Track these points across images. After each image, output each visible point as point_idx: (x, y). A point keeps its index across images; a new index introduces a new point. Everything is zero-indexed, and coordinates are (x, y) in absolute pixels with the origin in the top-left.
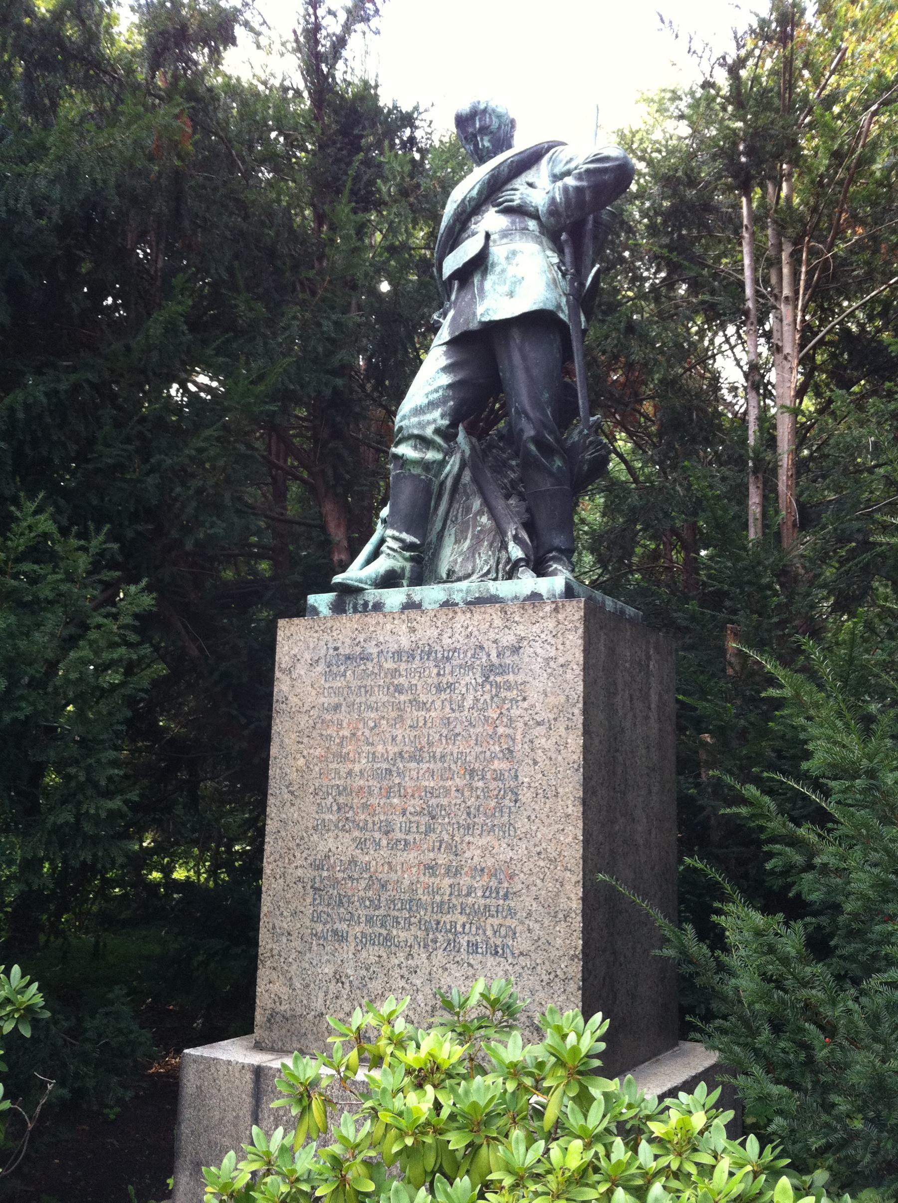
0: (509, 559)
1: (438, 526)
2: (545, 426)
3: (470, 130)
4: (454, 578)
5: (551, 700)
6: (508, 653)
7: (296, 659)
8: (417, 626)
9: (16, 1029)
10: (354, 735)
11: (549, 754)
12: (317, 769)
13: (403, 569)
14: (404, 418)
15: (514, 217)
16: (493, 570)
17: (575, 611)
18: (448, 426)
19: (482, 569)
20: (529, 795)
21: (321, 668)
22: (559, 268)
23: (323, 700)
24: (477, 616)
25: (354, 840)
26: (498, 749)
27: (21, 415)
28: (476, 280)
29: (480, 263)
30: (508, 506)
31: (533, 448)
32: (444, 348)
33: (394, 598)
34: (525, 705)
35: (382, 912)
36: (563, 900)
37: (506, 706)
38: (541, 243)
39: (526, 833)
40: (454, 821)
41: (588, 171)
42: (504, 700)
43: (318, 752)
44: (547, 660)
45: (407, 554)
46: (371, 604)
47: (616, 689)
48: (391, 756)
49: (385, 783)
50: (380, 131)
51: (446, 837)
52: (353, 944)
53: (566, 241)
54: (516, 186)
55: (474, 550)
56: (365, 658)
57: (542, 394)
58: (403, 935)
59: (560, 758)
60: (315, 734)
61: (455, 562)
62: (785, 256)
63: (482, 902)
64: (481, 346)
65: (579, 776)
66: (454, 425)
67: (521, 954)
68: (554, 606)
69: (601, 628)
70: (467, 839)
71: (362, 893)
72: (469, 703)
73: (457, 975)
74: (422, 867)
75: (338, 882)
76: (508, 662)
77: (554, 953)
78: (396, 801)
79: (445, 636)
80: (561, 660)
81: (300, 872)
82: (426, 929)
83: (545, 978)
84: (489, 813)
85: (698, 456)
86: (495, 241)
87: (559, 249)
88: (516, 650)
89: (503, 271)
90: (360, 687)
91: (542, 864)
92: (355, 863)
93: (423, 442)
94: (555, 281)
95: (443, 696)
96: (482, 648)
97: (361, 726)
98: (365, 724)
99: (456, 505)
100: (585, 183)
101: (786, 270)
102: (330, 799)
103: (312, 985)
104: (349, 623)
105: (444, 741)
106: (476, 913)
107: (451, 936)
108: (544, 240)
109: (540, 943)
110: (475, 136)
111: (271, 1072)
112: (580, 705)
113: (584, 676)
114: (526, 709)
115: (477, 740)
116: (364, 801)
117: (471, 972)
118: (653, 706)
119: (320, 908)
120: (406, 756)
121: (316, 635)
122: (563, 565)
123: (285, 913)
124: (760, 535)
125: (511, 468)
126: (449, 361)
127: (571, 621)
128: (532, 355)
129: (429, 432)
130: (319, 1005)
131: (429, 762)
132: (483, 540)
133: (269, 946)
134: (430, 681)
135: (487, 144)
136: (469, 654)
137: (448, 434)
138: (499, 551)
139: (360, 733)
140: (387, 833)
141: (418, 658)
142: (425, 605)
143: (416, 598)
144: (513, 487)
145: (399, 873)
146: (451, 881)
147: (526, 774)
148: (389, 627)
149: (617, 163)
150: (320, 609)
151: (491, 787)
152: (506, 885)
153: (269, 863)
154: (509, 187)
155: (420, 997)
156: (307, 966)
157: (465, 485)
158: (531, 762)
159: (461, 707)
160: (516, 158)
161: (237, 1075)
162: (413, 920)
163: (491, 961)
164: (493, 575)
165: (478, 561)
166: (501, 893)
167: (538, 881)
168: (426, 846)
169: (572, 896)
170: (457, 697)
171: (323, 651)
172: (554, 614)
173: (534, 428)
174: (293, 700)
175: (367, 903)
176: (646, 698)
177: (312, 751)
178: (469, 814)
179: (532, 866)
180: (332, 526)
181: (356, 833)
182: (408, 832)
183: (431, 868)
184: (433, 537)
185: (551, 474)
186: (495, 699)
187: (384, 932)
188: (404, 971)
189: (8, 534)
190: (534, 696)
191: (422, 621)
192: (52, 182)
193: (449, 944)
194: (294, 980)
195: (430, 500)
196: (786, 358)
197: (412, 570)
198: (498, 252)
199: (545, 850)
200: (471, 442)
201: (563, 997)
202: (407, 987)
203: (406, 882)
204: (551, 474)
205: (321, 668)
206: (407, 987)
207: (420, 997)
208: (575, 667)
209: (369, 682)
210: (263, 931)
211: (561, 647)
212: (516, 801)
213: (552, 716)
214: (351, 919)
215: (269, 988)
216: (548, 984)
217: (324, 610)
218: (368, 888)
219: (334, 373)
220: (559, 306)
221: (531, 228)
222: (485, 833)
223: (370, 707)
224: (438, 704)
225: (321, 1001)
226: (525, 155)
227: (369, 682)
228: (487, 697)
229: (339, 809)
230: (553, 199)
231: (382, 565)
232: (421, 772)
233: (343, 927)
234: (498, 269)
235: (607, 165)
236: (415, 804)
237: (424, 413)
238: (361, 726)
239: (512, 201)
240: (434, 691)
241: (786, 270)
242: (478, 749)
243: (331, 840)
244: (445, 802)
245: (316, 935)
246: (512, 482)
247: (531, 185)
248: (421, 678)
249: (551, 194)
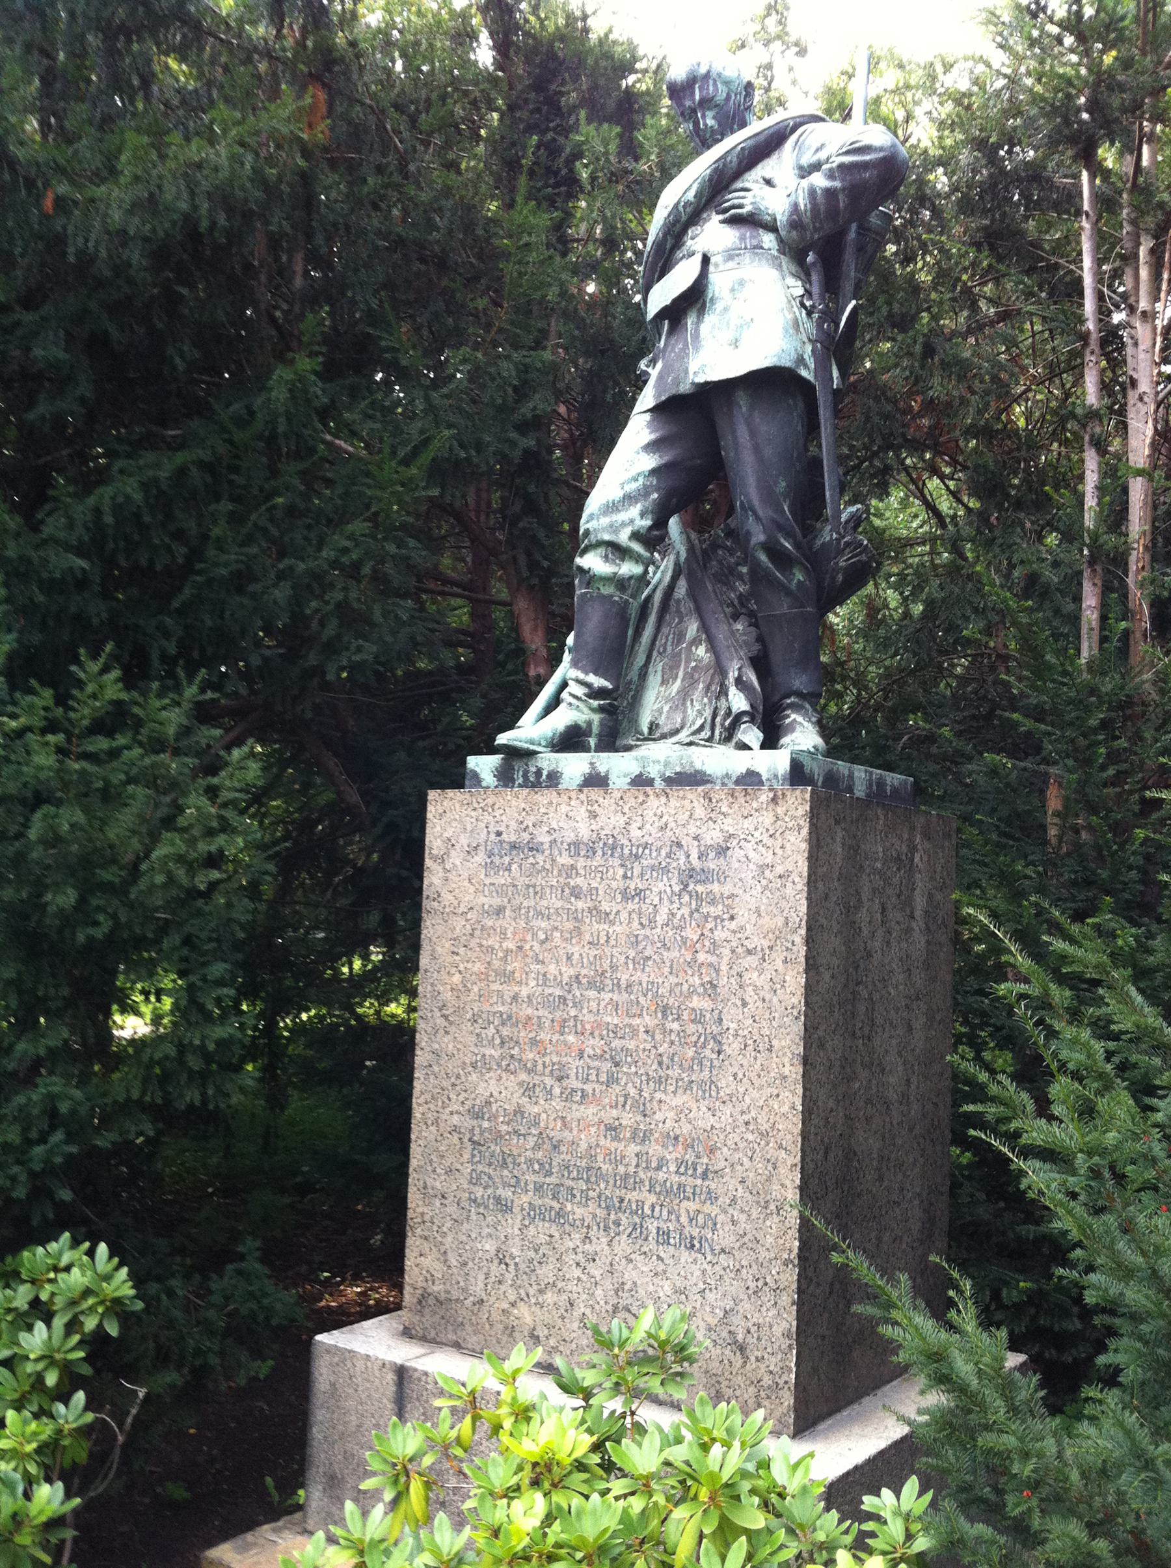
0: (729, 712)
1: (640, 659)
2: (780, 528)
3: (688, 103)
4: (657, 735)
5: (766, 921)
6: (712, 855)
8: (599, 811)
9: (100, 1326)
10: (520, 948)
11: (762, 994)
12: (476, 989)
13: (589, 723)
14: (591, 517)
15: (743, 230)
16: (708, 726)
17: (798, 803)
18: (650, 528)
21: (480, 858)
22: (803, 305)
23: (483, 900)
24: (673, 802)
25: (521, 1084)
26: (698, 982)
27: (109, 519)
28: (690, 321)
29: (694, 298)
30: (733, 633)
31: (763, 557)
32: (647, 417)
33: (574, 766)
34: (733, 925)
35: (553, 1179)
37: (709, 926)
38: (779, 267)
39: (731, 1096)
40: (642, 1071)
41: (842, 166)
42: (706, 917)
43: (478, 967)
44: (762, 868)
45: (595, 703)
46: (545, 773)
47: (859, 900)
48: (565, 979)
49: (558, 1014)
50: (584, 87)
51: (633, 1092)
52: (520, 1217)
53: (813, 264)
54: (747, 185)
55: (685, 694)
56: (534, 848)
57: (776, 483)
58: (579, 1212)
59: (775, 1000)
60: (473, 943)
61: (660, 711)
62: (1143, 252)
63: (676, 1179)
64: (697, 413)
65: (799, 1027)
66: (660, 523)
67: (723, 1251)
68: (771, 795)
69: (837, 822)
70: (658, 1095)
71: (528, 1153)
72: (662, 918)
73: (645, 1269)
74: (602, 1127)
75: (501, 1137)
76: (712, 866)
77: (764, 1255)
78: (571, 1038)
79: (634, 826)
80: (780, 870)
81: (455, 1119)
82: (607, 1207)
83: (752, 1285)
84: (686, 1065)
85: (1023, 528)
86: (716, 265)
87: (804, 272)
88: (722, 851)
89: (726, 309)
90: (528, 886)
91: (751, 1137)
92: (522, 1113)
93: (618, 551)
94: (796, 324)
95: (631, 906)
96: (679, 845)
97: (529, 937)
98: (535, 935)
99: (665, 630)
100: (837, 184)
101: (1144, 273)
102: (492, 1030)
103: (470, 1264)
104: (515, 801)
105: (631, 966)
106: (667, 1192)
107: (637, 1220)
108: (784, 260)
109: (746, 1239)
110: (694, 111)
111: (416, 1375)
112: (803, 932)
113: (809, 893)
114: (734, 932)
115: (671, 967)
116: (532, 1035)
117: (661, 1267)
118: (918, 913)
119: (480, 1168)
120: (584, 981)
121: (474, 814)
122: (805, 715)
123: (439, 1170)
124: (1096, 652)
125: (740, 577)
126: (653, 437)
127: (793, 818)
128: (764, 428)
129: (623, 537)
130: (478, 1288)
131: (612, 991)
132: (697, 681)
133: (420, 1210)
134: (614, 884)
135: (710, 122)
136: (663, 853)
137: (653, 538)
138: (718, 698)
139: (527, 947)
140: (560, 1079)
141: (600, 852)
142: (613, 778)
143: (602, 769)
144: (742, 605)
145: (575, 1132)
146: (638, 1148)
147: (732, 1017)
148: (564, 808)
149: (882, 154)
150: (482, 776)
151: (689, 1032)
152: (705, 1160)
153: (419, 1105)
154: (739, 184)
155: (599, 1292)
156: (464, 1238)
157: (678, 601)
158: (739, 1003)
159: (652, 921)
160: (749, 143)
161: (377, 1373)
162: (591, 1194)
163: (685, 1256)
164: (706, 734)
165: (689, 711)
166: (699, 1171)
167: (746, 1160)
168: (607, 1101)
169: (788, 1183)
170: (647, 909)
171: (483, 836)
172: (771, 806)
173: (765, 532)
174: (447, 897)
175: (536, 1167)
176: (907, 904)
177: (469, 966)
178: (660, 1064)
179: (737, 1139)
180: (526, 630)
181: (523, 1076)
182: (586, 1080)
183: (613, 1130)
184: (634, 674)
185: (788, 592)
186: (696, 915)
187: (557, 1206)
188: (580, 1258)
189: (71, 703)
190: (744, 916)
191: (605, 803)
192: (130, 212)
193: (634, 1229)
194: (450, 1254)
195: (627, 627)
196: (1141, 399)
197: (601, 724)
198: (718, 282)
199: (755, 1119)
200: (688, 537)
201: (773, 1312)
202: (584, 1278)
203: (584, 1146)
204: (788, 592)
205: (480, 858)
206: (584, 1278)
207: (599, 1292)
208: (797, 879)
209: (539, 880)
210: (412, 1190)
211: (779, 852)
212: (719, 1052)
213: (766, 943)
214: (517, 1184)
215: (421, 1262)
216: (755, 1292)
217: (488, 779)
218: (537, 1147)
219: (524, 427)
220: (801, 360)
221: (766, 246)
222: (680, 1091)
223: (540, 914)
224: (624, 915)
225: (481, 1285)
226: (762, 138)
227: (539, 880)
228: (685, 911)
229: (503, 1043)
230: (796, 205)
231: (562, 718)
232: (603, 1004)
233: (507, 1193)
234: (719, 306)
235: (867, 158)
236: (594, 1045)
237: (618, 511)
238: (529, 937)
239: (741, 206)
240: (619, 897)
241: (1144, 273)
242: (673, 980)
243: (492, 1082)
244: (631, 1045)
245: (475, 1201)
246: (741, 596)
247: (768, 182)
248: (604, 879)
249: (793, 197)
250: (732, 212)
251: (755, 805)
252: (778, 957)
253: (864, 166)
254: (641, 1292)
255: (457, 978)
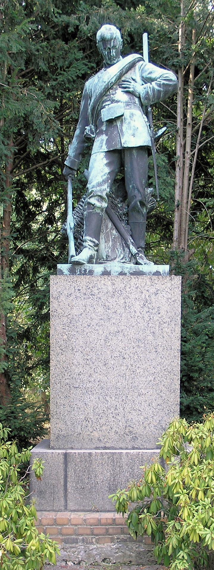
7: (60, 293)
8: (115, 283)
19: (120, 256)
20: (161, 349)
24: (140, 280)
33: (98, 269)
34: (160, 315)
36: (173, 385)
39: (160, 363)
44: (168, 299)
46: (88, 271)
80: (173, 299)
81: (67, 381)
83: (167, 412)
91: (166, 373)
117: (140, 412)
127: (177, 284)
142: (112, 273)
143: (108, 270)
148: (103, 282)
150: (64, 271)
155: (120, 423)
174: (59, 311)
188: (114, 415)
190: (163, 312)
207: (120, 423)
213: (169, 320)
217: (66, 272)
225: (79, 428)
234: (127, 121)
239: (129, 88)
250: (127, 89)
251: (165, 281)
252: (173, 323)
253: (170, 85)
254: (134, 421)
255: (65, 337)
